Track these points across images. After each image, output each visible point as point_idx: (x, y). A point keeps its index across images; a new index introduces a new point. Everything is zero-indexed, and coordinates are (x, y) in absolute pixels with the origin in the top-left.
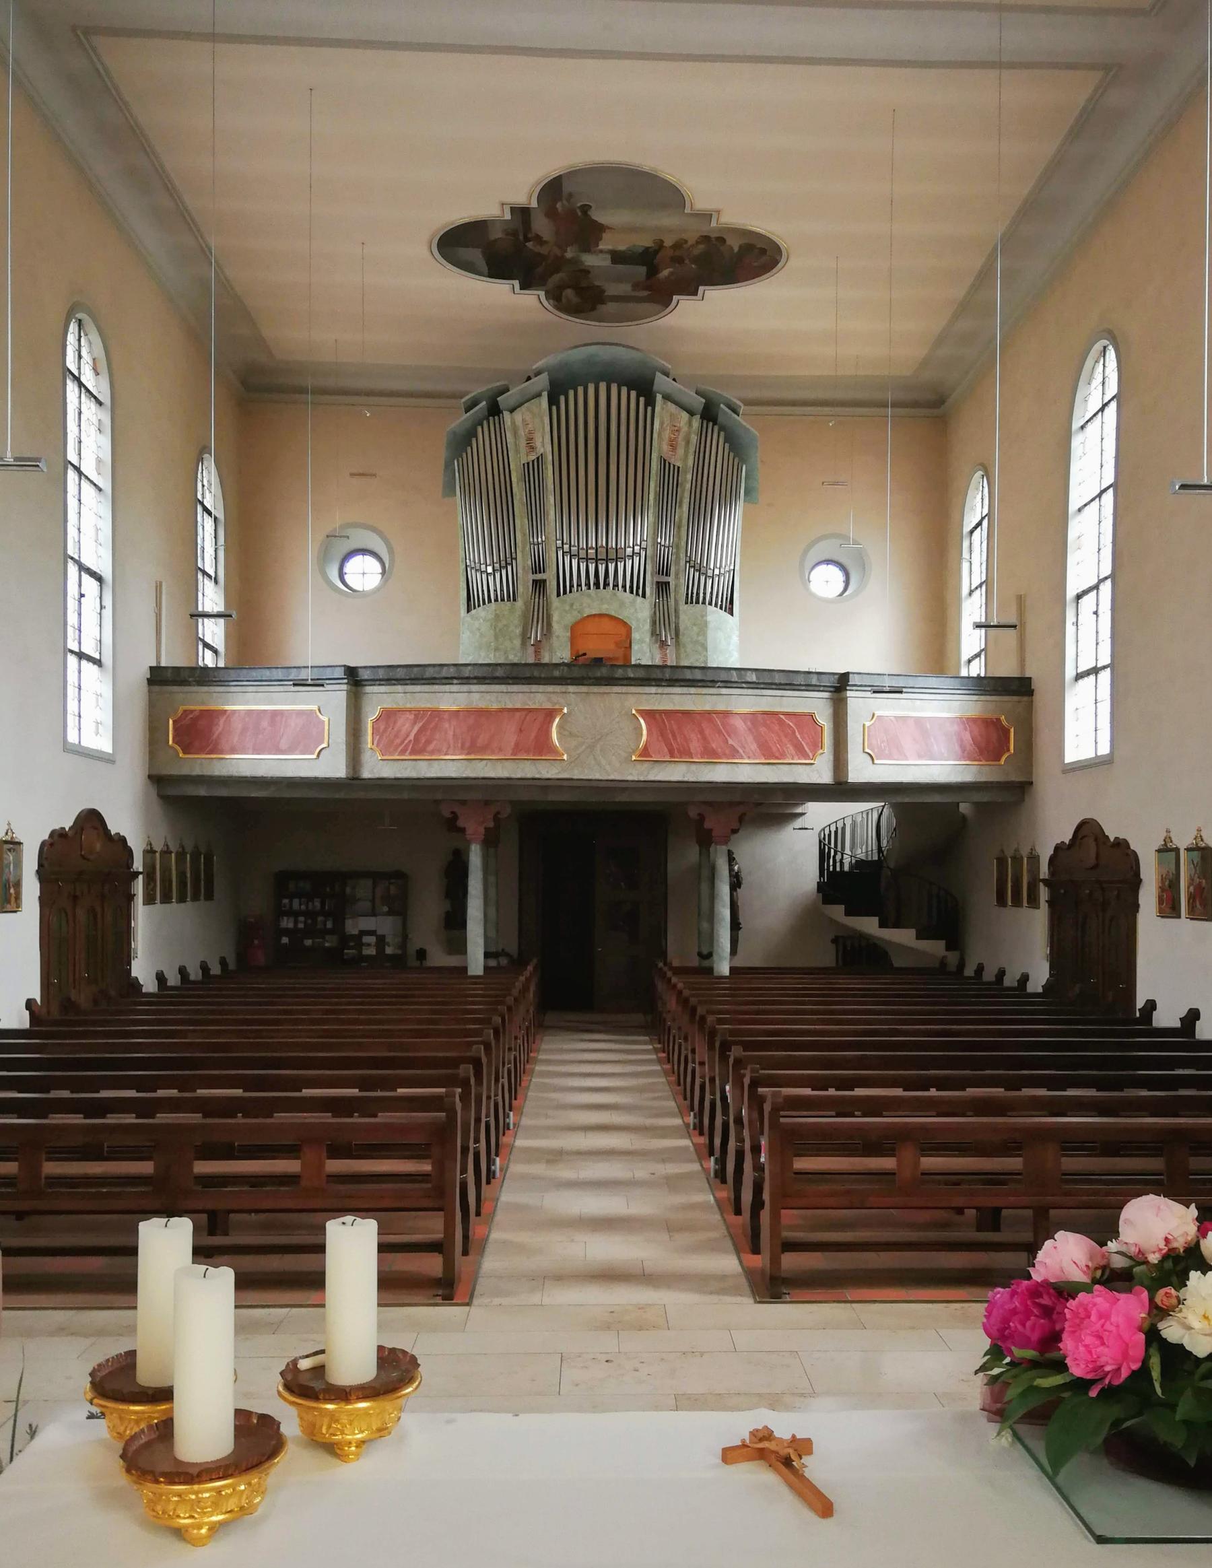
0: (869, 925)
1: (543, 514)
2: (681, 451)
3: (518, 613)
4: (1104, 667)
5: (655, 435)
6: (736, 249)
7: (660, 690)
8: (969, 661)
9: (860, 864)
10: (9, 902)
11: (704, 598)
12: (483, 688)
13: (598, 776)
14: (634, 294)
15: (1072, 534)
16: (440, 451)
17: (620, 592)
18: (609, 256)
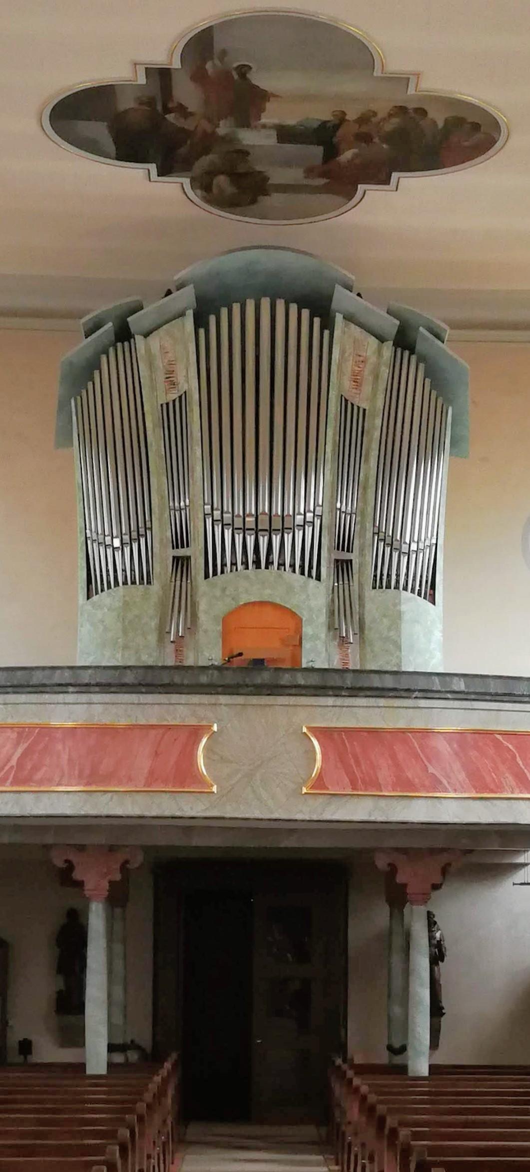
2: (367, 389)
3: (154, 599)
6: (441, 124)
7: (339, 701)
11: (398, 582)
13: (257, 814)
16: (52, 387)
18: (274, 133)
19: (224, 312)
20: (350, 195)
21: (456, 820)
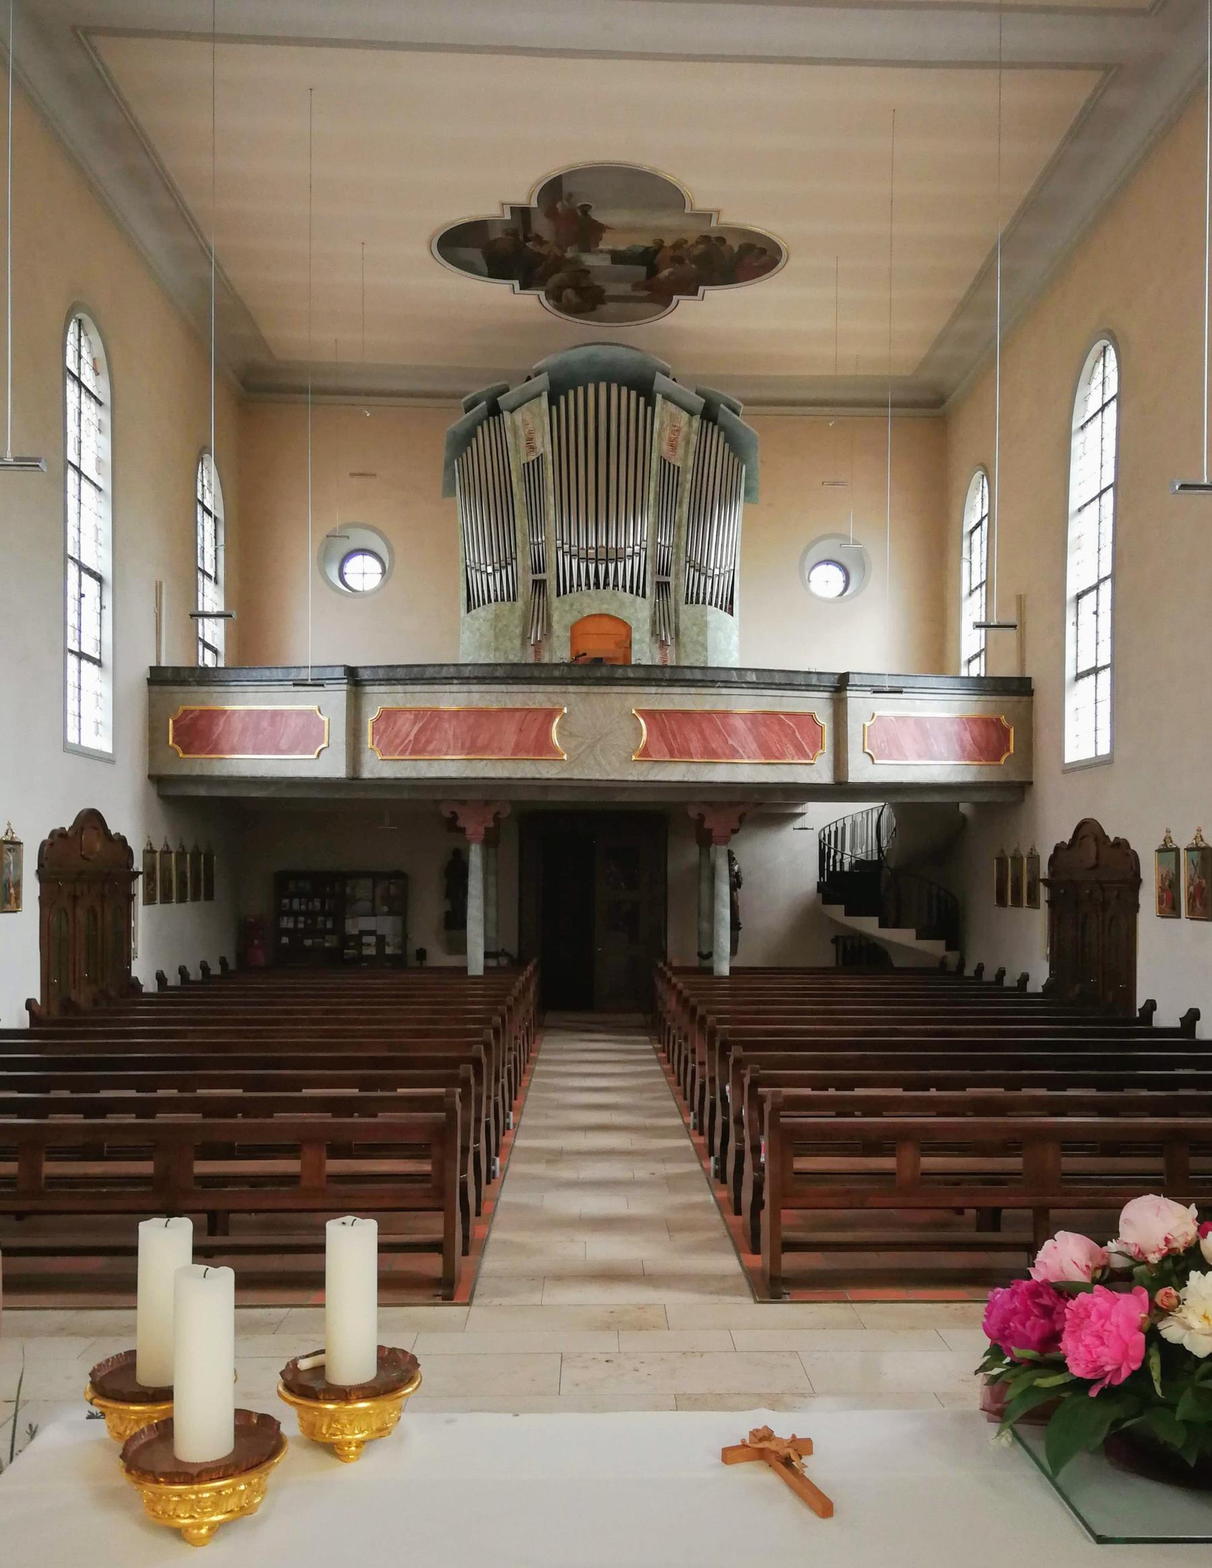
0: (869, 925)
1: (543, 514)
2: (681, 451)
3: (518, 613)
4: (1104, 667)
5: (655, 435)
6: (736, 249)
7: (660, 690)
8: (969, 661)
9: (860, 864)
10: (9, 902)
11: (704, 598)
12: (483, 688)
13: (598, 776)
14: (634, 294)
15: (1072, 534)
16: (440, 451)
17: (620, 592)
18: (609, 256)
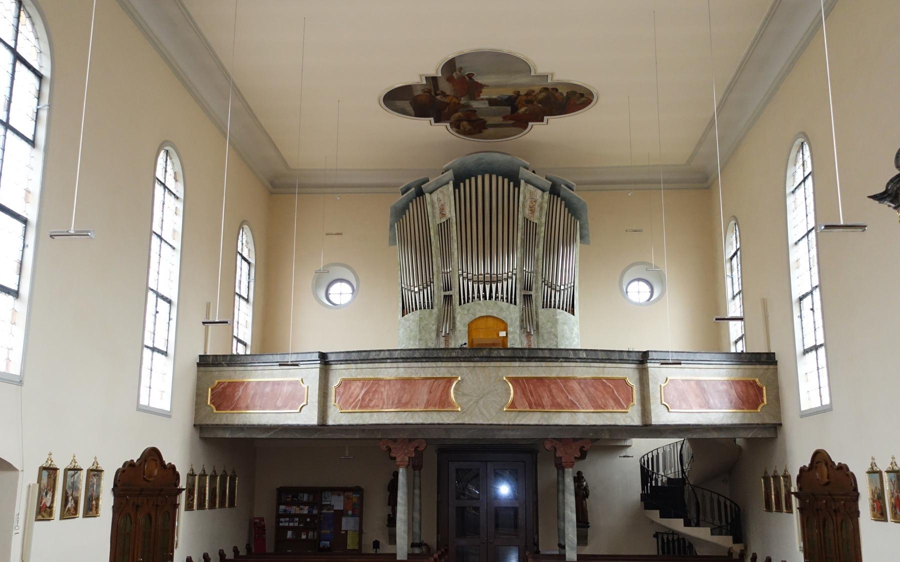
0: (677, 525)
1: (450, 255)
2: (537, 214)
3: (435, 316)
4: (821, 345)
5: (521, 205)
6: (565, 94)
7: (522, 364)
8: (736, 342)
10: (91, 510)
12: (406, 364)
13: (481, 422)
14: (505, 122)
15: (792, 259)
16: (386, 218)
17: (499, 302)
18: (487, 102)
19: (467, 181)
20: (526, 128)
21: (584, 424)
